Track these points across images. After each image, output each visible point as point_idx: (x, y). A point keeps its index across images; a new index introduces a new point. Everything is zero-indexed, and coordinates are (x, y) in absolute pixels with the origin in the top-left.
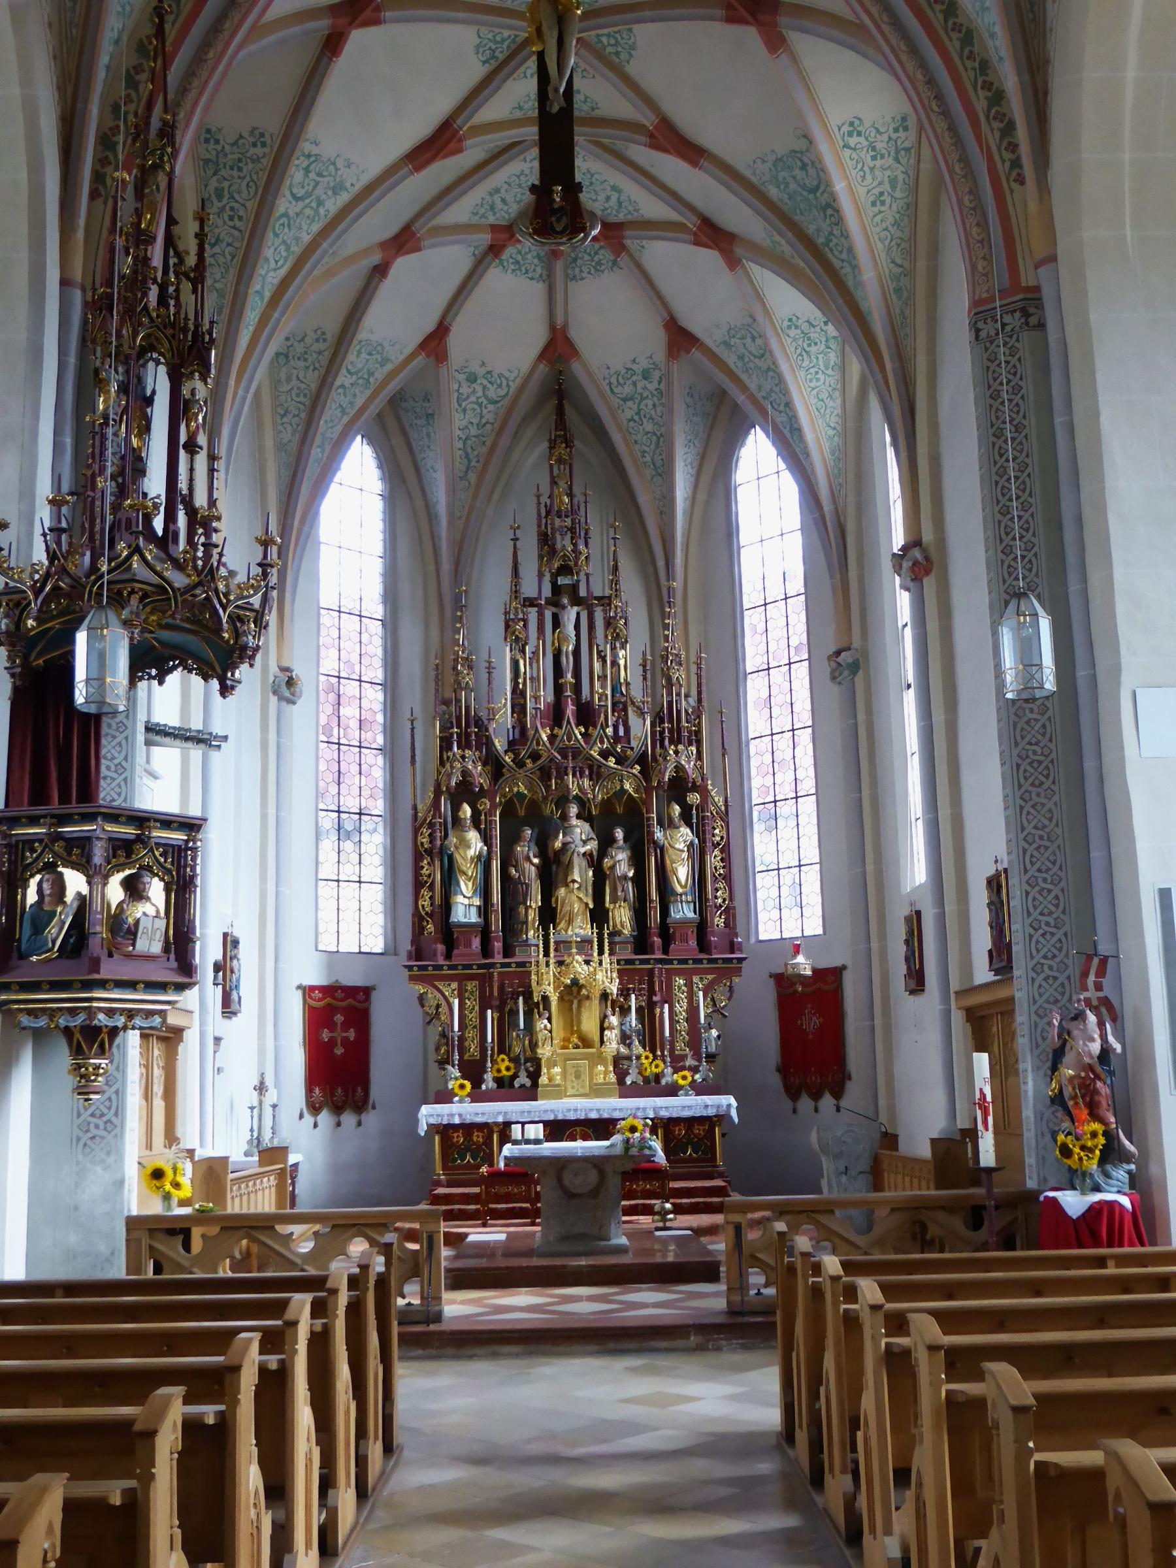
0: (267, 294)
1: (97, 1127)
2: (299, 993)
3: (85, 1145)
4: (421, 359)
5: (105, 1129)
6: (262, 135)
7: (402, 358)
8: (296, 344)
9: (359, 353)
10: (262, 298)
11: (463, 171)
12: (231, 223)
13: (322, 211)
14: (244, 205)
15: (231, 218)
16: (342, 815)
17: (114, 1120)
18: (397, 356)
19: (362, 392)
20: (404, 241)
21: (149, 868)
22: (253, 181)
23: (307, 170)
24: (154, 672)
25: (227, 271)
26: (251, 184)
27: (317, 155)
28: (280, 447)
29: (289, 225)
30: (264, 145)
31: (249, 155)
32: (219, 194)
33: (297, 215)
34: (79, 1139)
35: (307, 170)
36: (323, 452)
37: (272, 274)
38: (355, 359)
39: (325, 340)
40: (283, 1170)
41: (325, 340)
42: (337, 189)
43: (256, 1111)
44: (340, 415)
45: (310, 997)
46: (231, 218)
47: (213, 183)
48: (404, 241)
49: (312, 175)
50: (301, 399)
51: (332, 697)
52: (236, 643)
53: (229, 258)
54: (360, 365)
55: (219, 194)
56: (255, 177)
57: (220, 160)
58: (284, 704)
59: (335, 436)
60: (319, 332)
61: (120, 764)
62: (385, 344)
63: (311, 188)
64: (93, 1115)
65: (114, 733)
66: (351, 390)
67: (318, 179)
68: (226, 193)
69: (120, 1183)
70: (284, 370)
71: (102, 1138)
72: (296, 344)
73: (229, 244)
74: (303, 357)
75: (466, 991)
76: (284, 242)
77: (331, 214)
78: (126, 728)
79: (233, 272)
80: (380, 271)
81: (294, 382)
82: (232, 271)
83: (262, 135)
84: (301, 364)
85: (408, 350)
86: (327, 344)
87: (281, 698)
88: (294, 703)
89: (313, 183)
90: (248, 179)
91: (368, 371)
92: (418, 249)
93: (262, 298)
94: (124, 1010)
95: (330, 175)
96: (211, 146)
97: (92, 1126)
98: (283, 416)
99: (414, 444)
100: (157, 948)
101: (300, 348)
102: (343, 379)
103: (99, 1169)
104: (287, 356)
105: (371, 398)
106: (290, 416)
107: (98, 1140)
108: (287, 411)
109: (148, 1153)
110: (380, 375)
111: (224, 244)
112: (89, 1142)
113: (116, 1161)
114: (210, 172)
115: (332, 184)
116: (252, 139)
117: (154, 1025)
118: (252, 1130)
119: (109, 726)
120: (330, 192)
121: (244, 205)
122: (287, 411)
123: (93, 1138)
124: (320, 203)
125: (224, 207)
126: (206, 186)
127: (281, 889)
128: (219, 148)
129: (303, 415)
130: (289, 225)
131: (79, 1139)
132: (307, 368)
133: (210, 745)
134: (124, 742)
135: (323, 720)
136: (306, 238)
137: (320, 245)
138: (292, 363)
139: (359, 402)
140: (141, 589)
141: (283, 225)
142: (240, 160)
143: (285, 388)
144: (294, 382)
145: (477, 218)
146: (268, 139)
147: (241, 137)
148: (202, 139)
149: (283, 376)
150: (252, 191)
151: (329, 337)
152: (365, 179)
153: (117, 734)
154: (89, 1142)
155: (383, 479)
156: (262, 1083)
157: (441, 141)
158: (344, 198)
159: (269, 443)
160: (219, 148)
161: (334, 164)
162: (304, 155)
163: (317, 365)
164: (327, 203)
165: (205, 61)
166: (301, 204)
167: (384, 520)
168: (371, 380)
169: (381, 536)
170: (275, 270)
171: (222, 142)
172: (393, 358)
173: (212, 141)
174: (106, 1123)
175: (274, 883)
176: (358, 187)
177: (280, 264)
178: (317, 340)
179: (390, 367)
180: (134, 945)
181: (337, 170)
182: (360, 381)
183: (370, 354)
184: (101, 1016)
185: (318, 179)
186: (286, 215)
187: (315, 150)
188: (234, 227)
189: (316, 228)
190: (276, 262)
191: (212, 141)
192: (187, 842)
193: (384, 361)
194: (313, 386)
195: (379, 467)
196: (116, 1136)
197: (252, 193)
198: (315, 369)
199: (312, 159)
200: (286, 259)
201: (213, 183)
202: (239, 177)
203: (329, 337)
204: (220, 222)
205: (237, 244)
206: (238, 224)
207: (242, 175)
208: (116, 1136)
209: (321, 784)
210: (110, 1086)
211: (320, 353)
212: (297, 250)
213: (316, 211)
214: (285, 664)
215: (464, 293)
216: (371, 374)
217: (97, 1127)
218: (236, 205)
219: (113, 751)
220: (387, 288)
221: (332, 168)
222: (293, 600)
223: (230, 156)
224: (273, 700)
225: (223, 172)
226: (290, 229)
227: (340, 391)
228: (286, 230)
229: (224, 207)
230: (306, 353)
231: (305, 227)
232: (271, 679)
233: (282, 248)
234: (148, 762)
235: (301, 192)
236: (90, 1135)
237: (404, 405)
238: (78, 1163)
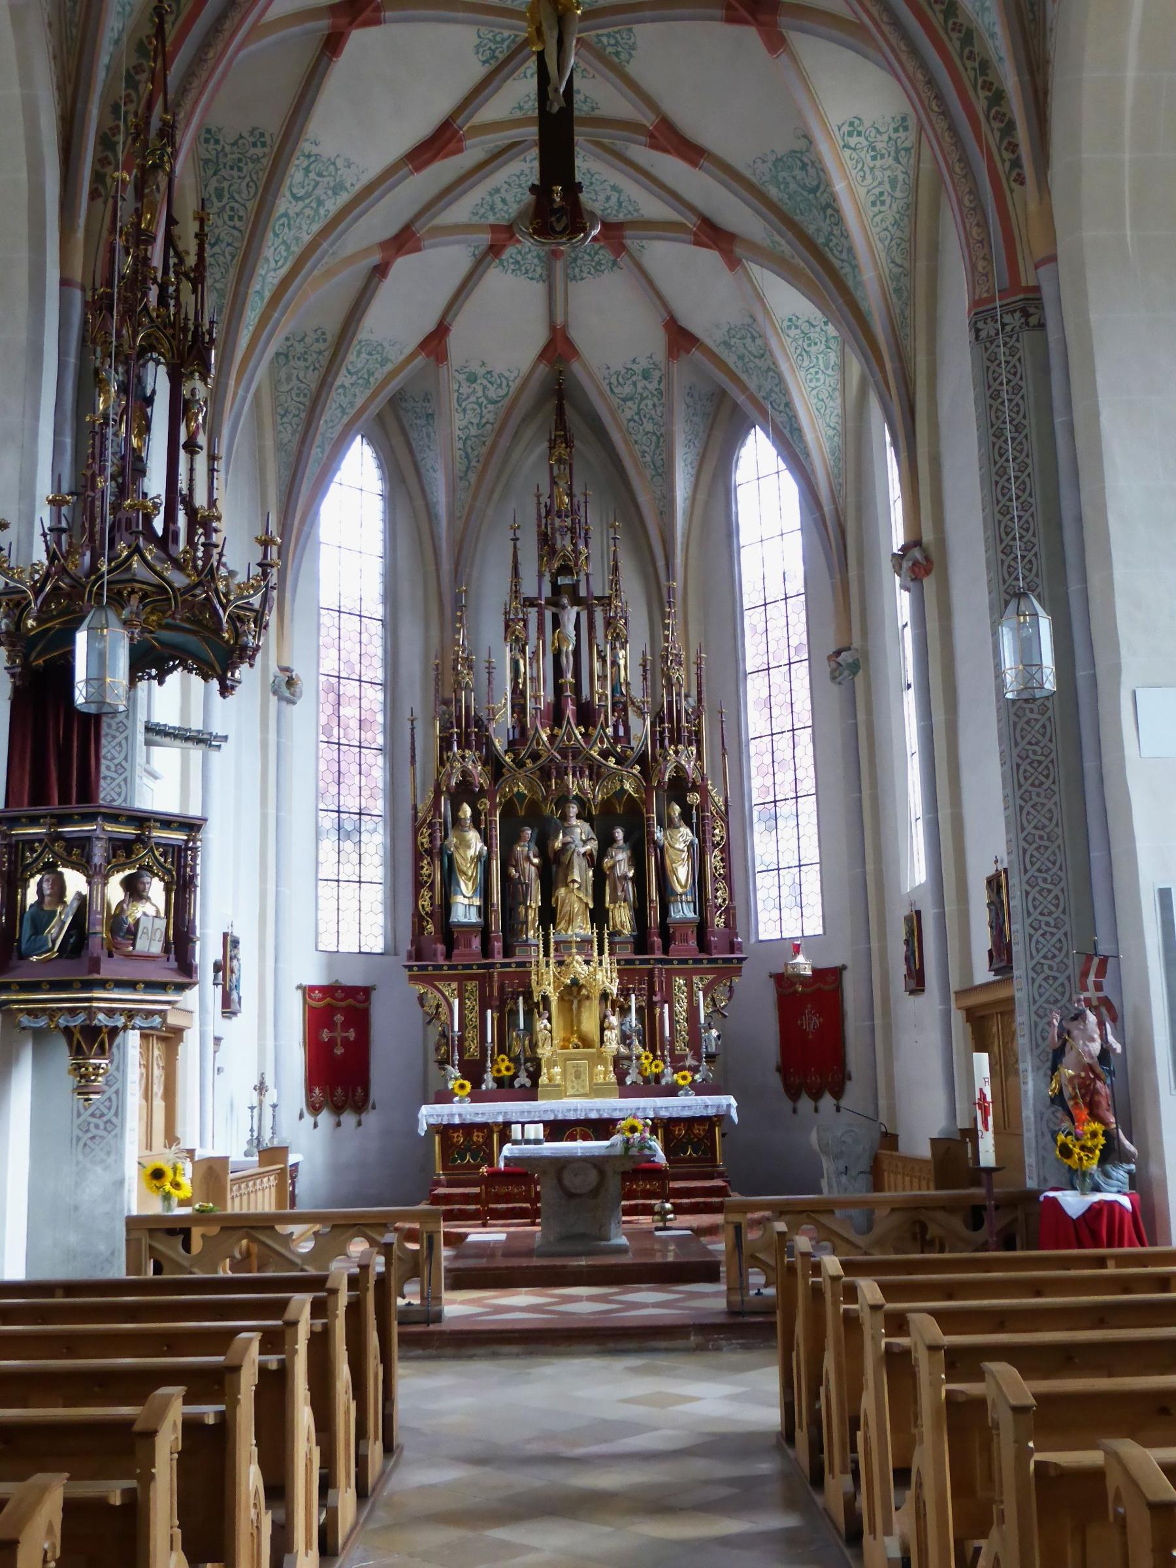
0: (267, 294)
1: (97, 1127)
2: (299, 993)
3: (85, 1145)
4: (421, 359)
5: (105, 1129)
6: (262, 135)
7: (402, 358)
8: (296, 344)
9: (359, 353)
10: (262, 298)
11: (463, 171)
12: (231, 223)
13: (322, 211)
14: (244, 205)
15: (231, 218)
16: (342, 815)
17: (114, 1120)
18: (397, 356)
19: (362, 392)
20: (404, 241)
21: (149, 868)
22: (253, 181)
23: (307, 170)
24: (154, 672)
25: (227, 271)
26: (251, 184)
27: (317, 155)
28: (280, 447)
29: (289, 225)
30: (264, 145)
31: (249, 155)
32: (219, 194)
33: (297, 215)
34: (79, 1139)
35: (307, 170)
37: (272, 274)
39: (325, 340)
40: (283, 1170)
41: (325, 340)
42: (337, 189)
43: (256, 1111)
44: (340, 415)
45: (310, 997)
46: (231, 218)
47: (213, 183)
48: (404, 241)
49: (312, 175)
50: (301, 399)
51: (332, 697)
53: (229, 258)
54: (360, 365)
55: (219, 194)
56: (255, 177)
58: (284, 704)
59: (335, 436)
60: (319, 332)
61: (120, 764)
62: (385, 344)
63: (311, 188)
64: (93, 1115)
65: (114, 733)
66: (351, 390)
67: (318, 179)
68: (226, 193)
70: (284, 370)
71: (102, 1138)
72: (296, 344)
73: (229, 244)
74: (303, 357)
76: (284, 242)
77: (331, 214)
78: (126, 728)
79: (233, 272)
80: (380, 271)
81: (294, 382)
82: (232, 271)
83: (262, 135)
84: (301, 364)
85: (408, 350)
86: (327, 344)
87: (281, 698)
88: (294, 703)
89: (313, 183)
90: (248, 179)
91: (368, 371)
92: (418, 249)
93: (262, 298)
94: (124, 1010)
95: (330, 175)
96: (211, 146)
97: (92, 1126)
98: (283, 416)
99: (414, 444)
100: (157, 948)
101: (300, 348)
102: (343, 379)
103: (99, 1169)
104: (287, 356)
105: (371, 398)
106: (290, 416)
107: (98, 1140)
108: (287, 411)
110: (380, 375)
111: (224, 244)
112: (89, 1142)
113: (116, 1161)
114: (210, 172)
115: (332, 184)
116: (252, 139)
117: (154, 1025)
118: (252, 1130)
119: (109, 726)
120: (330, 192)
121: (244, 205)
122: (287, 411)
123: (93, 1138)
124: (320, 203)
125: (224, 207)
126: (206, 186)
127: (281, 889)
128: (219, 148)
129: (303, 415)
130: (289, 225)
131: (79, 1139)
132: (307, 368)
133: (210, 745)
134: (124, 742)
135: (323, 720)
136: (306, 238)
137: (320, 245)
138: (292, 363)
139: (359, 402)
140: (141, 589)
141: (283, 225)
142: (240, 160)
143: (285, 388)
144: (294, 382)
145: (477, 218)
146: (268, 139)
147: (241, 137)
148: (202, 139)
149: (283, 376)
150: (252, 191)
151: (329, 337)
152: (365, 179)
153: (117, 734)
154: (89, 1142)
155: (383, 479)
156: (262, 1083)
158: (344, 198)
159: (269, 443)
160: (219, 148)
161: (334, 164)
162: (304, 155)
163: (317, 365)
164: (327, 203)
165: (205, 61)
166: (301, 204)
167: (384, 520)
168: (371, 380)
169: (381, 536)
170: (275, 270)
171: (222, 142)
172: (393, 358)
173: (212, 141)
174: (106, 1123)
175: (274, 883)
176: (358, 187)
177: (280, 264)
178: (317, 340)
179: (390, 367)
180: (134, 945)
182: (360, 381)
183: (370, 354)
184: (101, 1016)
185: (318, 179)
186: (286, 215)
187: (315, 150)
188: (234, 227)
189: (316, 228)
190: (276, 262)
191: (212, 141)
192: (187, 842)
193: (384, 361)
194: (313, 386)
195: (379, 467)
196: (116, 1136)
197: (252, 193)
198: (315, 369)
199: (312, 159)
201: (213, 183)
202: (239, 177)
203: (329, 337)
204: (220, 222)
205: (237, 244)
206: (238, 224)
207: (242, 175)
208: (116, 1136)
209: (321, 784)
210: (110, 1086)
211: (320, 353)
212: (297, 250)
213: (316, 211)
214: (285, 664)
216: (371, 374)
217: (97, 1127)
218: (236, 205)
219: (113, 751)
220: (387, 288)
221: (332, 168)
222: (293, 600)
223: (230, 156)
224: (273, 700)
225: (223, 172)
226: (290, 229)
227: (340, 391)
228: (286, 230)
229: (224, 207)
230: (306, 353)
231: (305, 227)
232: (271, 679)
233: (282, 248)
234: (148, 762)
235: (301, 192)
236: (90, 1135)
237: (404, 405)
238: (78, 1163)
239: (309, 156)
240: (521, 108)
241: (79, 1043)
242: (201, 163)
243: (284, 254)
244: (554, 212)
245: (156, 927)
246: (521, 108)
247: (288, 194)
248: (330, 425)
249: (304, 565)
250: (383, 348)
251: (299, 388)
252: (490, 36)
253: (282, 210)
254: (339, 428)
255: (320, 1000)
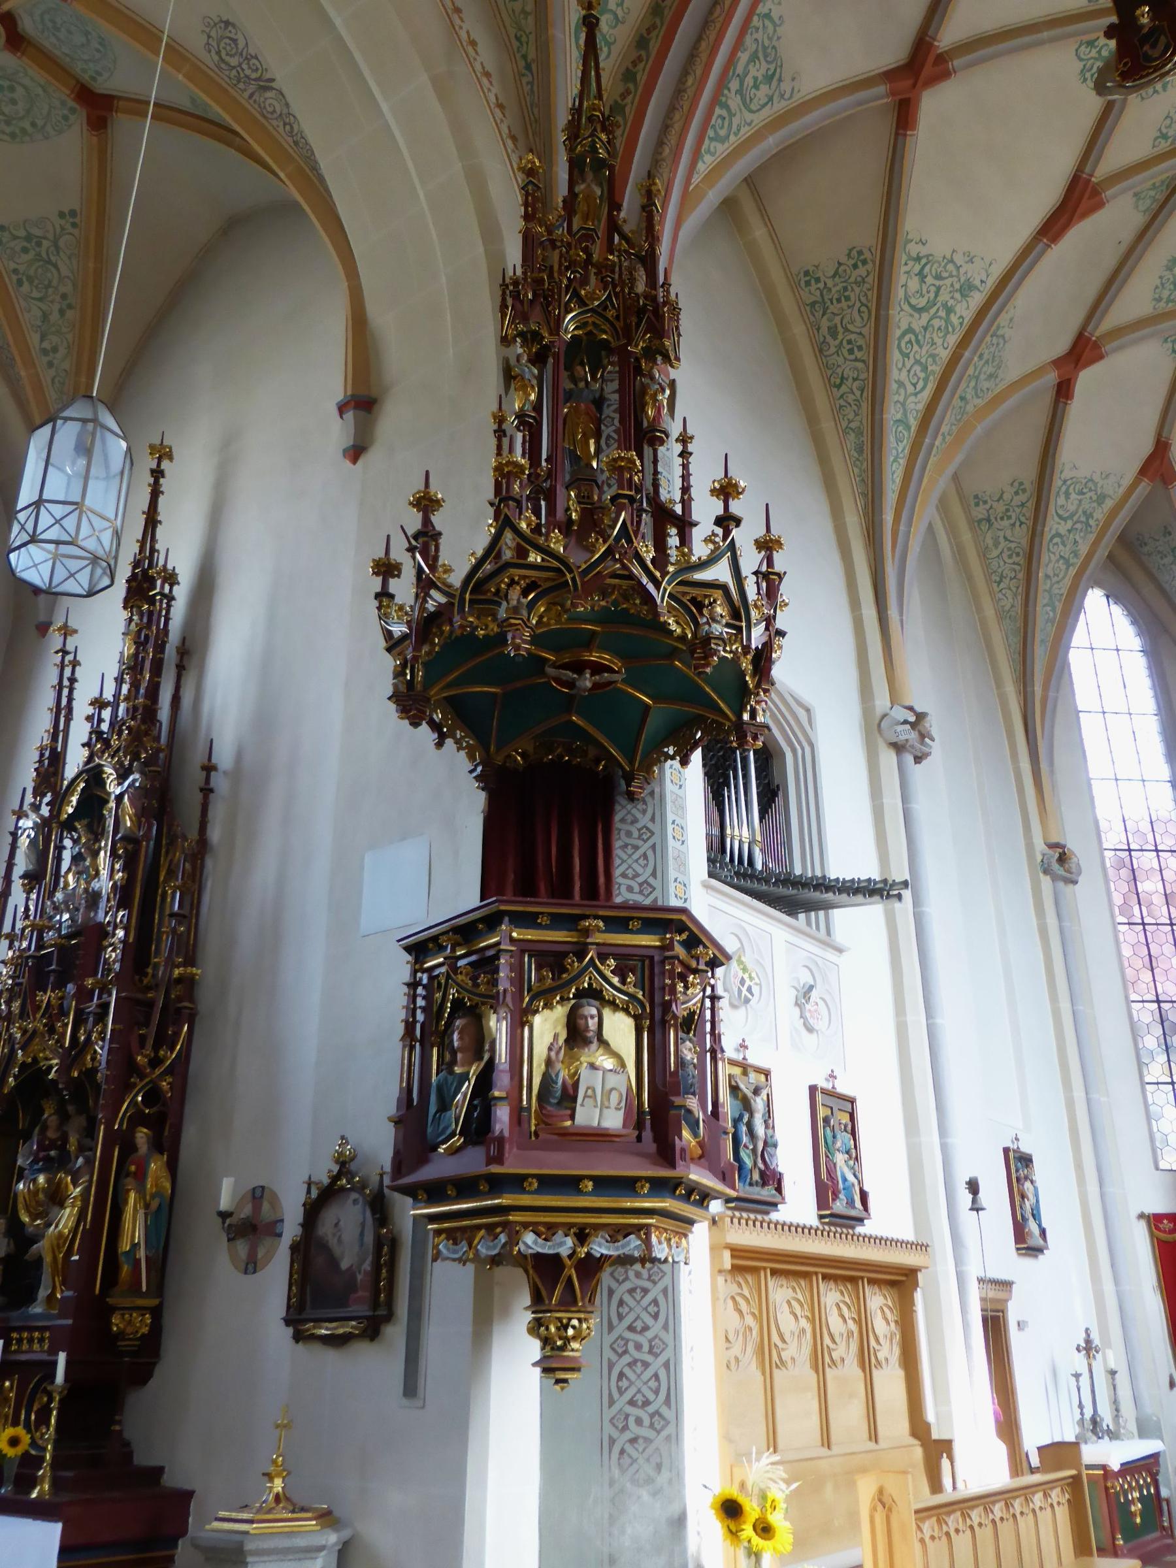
0: (914, 423)
1: (639, 1421)
2: (1143, 1224)
3: (622, 1452)
4: (1145, 487)
5: (652, 1426)
6: (860, 253)
7: (1121, 491)
8: (995, 505)
9: (1067, 495)
10: (908, 428)
11: (1123, 248)
12: (852, 357)
13: (954, 319)
14: (860, 333)
15: (851, 351)
16: (1162, 1005)
17: (664, 1411)
18: (1114, 489)
19: (1084, 538)
20: (1083, 351)
21: (595, 994)
22: (863, 304)
23: (921, 276)
24: (671, 751)
25: (859, 407)
26: (863, 309)
27: (927, 256)
28: (1001, 615)
29: (918, 341)
30: (864, 262)
31: (852, 279)
32: (833, 331)
33: (925, 329)
34: (612, 1441)
35: (921, 276)
36: (1054, 610)
37: (912, 399)
38: (1058, 502)
39: (1024, 491)
40: (1075, 1482)
41: (1024, 491)
42: (966, 289)
43: (1085, 1381)
44: (1064, 567)
45: (1157, 1228)
46: (851, 351)
47: (825, 324)
48: (1083, 351)
49: (929, 280)
50: (1015, 559)
51: (1125, 873)
52: (695, 634)
53: (858, 393)
54: (1072, 508)
55: (833, 331)
56: (863, 299)
57: (826, 297)
58: (1061, 884)
59: (1064, 591)
60: (1016, 484)
61: (646, 882)
62: (1096, 478)
63: (932, 295)
64: (632, 1403)
65: (636, 842)
66: (1068, 536)
67: (937, 283)
68: (840, 329)
69: (680, 1522)
70: (989, 535)
71: (648, 1441)
72: (995, 505)
73: (854, 380)
74: (1006, 515)
75: (424, 998)
76: (917, 362)
77: (967, 321)
78: (653, 833)
79: (865, 407)
80: (1064, 391)
81: (1003, 543)
82: (864, 405)
83: (860, 253)
84: (1006, 523)
85: (1127, 481)
86: (1028, 494)
87: (1055, 878)
88: (1075, 882)
89: (933, 289)
90: (858, 304)
91: (1084, 513)
92: (1101, 357)
93: (908, 428)
94: (570, 1226)
95: (951, 276)
96: (814, 286)
97: (631, 1420)
98: (999, 583)
99: (1166, 586)
100: (614, 1120)
101: (1000, 508)
102: (1053, 525)
103: (644, 1494)
104: (988, 520)
105: (1096, 544)
106: (1007, 581)
107: (641, 1445)
108: (1002, 577)
109: (871, 1445)
110: (1100, 514)
111: (850, 380)
112: (628, 1447)
113: (670, 1481)
114: (819, 314)
115: (957, 286)
116: (852, 262)
117: (626, 1251)
118: (1081, 1406)
119: (629, 834)
120: (958, 296)
121: (860, 333)
122: (1002, 577)
123: (633, 1441)
124: (950, 311)
125: (841, 342)
126: (818, 330)
127: (1094, 1096)
128: (821, 285)
129: (1021, 575)
130: (918, 341)
131: (612, 1441)
132: (1013, 525)
133: (888, 896)
134: (650, 854)
135: (1118, 900)
136: (944, 355)
137: (961, 356)
138: (996, 525)
139: (1084, 549)
140: (524, 577)
141: (910, 341)
142: (845, 289)
143: (995, 553)
144: (1003, 543)
145: (1162, 304)
146: (867, 255)
147: (840, 264)
148: (803, 284)
149: (989, 541)
150: (865, 316)
151: (1027, 485)
152: (997, 271)
153: (640, 843)
154: (628, 1447)
155: (1140, 634)
156: (1088, 1341)
157: (1078, 198)
158: (977, 299)
159: (990, 612)
160: (821, 285)
161: (952, 261)
162: (910, 258)
163: (1023, 519)
164: (958, 309)
165: (685, 91)
166: (925, 317)
167: (1151, 676)
168: (1091, 522)
169: (1150, 693)
170: (916, 394)
171: (822, 279)
172: (1111, 493)
173: (813, 281)
174: (652, 1416)
175: (1082, 1088)
176: (991, 283)
177: (920, 385)
178: (1017, 493)
179: (1109, 504)
180: (572, 1117)
181: (958, 268)
182: (1078, 526)
183: (1081, 493)
184: (529, 1238)
185: (937, 283)
186: (910, 330)
187: (924, 251)
188: (856, 360)
189: (953, 340)
190: (915, 385)
191: (813, 281)
192: (662, 948)
193: (1101, 499)
194: (1025, 542)
195: (1133, 623)
196: (668, 1438)
197: (866, 319)
198: (1021, 523)
199: (924, 261)
200: (926, 380)
201: (825, 324)
202: (849, 307)
203: (1027, 485)
204: (840, 360)
205: (862, 376)
206: (859, 354)
207: (850, 304)
208: (668, 1438)
209: (1128, 971)
210: (656, 1355)
211: (1023, 505)
212: (937, 369)
213: (948, 321)
214: (1054, 839)
215: (937, 18)
216: (1089, 516)
217: (639, 1421)
218: (853, 337)
219: (635, 866)
220: (1076, 407)
221: (950, 267)
222: (1052, 772)
223: (834, 290)
224: (1046, 881)
225: (832, 309)
226: (921, 347)
227: (1056, 540)
228: (916, 347)
229: (841, 342)
230: (1007, 510)
231: (939, 341)
232: (1039, 858)
233: (917, 368)
234: (829, 933)
235: (922, 302)
236: (628, 1435)
237: (1145, 549)
238: (612, 1483)
239: (918, 259)
240: (1164, 137)
241: (570, 1279)
242: (808, 308)
243: (922, 375)
244: (1145, 39)
245: (608, 1087)
246: (1164, 137)
247: (906, 307)
248: (1055, 579)
249: (1058, 732)
250: (1096, 484)
251: (1009, 549)
252: (1094, 53)
253: (904, 326)
254: (1067, 582)
255: (1171, 1232)
